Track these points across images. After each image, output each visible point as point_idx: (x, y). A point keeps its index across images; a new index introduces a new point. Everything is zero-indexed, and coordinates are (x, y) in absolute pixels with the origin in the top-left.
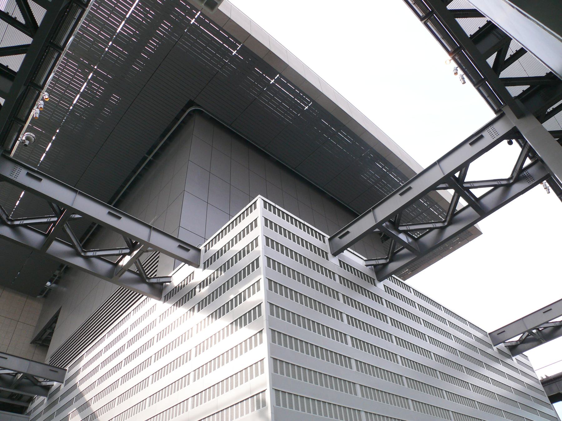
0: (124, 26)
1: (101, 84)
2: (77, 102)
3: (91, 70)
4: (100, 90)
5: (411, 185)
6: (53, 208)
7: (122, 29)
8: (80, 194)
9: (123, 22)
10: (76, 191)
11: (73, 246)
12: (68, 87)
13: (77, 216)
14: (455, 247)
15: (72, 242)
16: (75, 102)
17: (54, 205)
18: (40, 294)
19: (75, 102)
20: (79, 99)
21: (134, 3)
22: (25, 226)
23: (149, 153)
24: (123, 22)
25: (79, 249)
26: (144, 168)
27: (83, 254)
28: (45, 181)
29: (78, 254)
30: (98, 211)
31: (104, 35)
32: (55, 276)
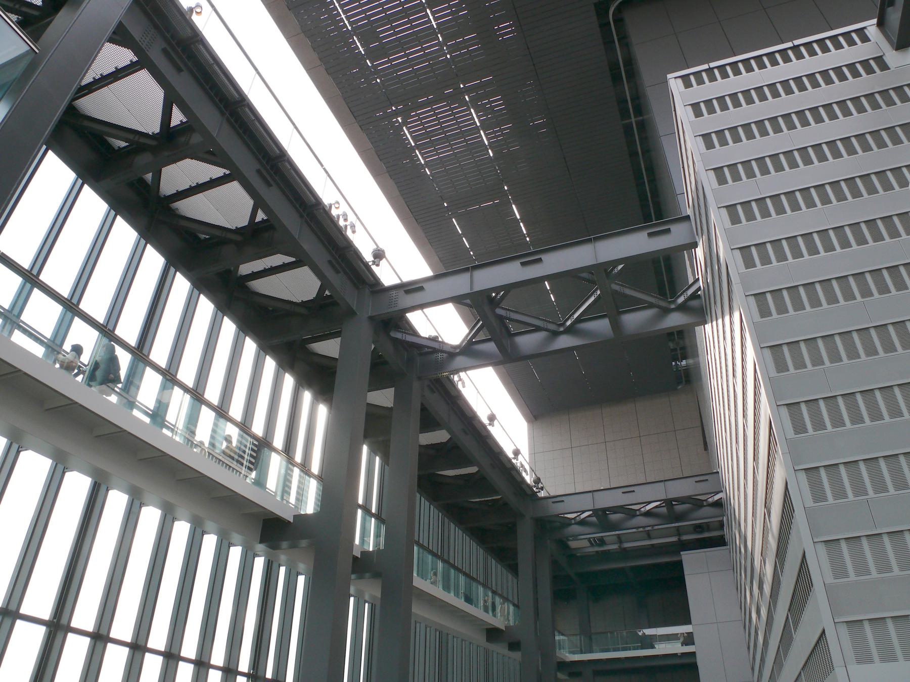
0: (433, 13)
1: (487, 96)
2: (488, 139)
3: (463, 92)
4: (497, 102)
5: (544, 257)
6: (584, 279)
7: (436, 19)
8: (596, 239)
9: (428, 11)
10: (589, 241)
11: (651, 306)
12: (463, 134)
13: (620, 267)
14: (782, 500)
15: (646, 302)
16: (486, 142)
17: (585, 275)
18: (679, 383)
19: (486, 142)
20: (486, 135)
21: (349, 22)
22: (579, 320)
23: (624, 114)
24: (428, 11)
25: (663, 304)
26: (640, 139)
27: (673, 306)
28: (546, 258)
29: (666, 311)
30: (635, 244)
31: (431, 47)
32: (675, 350)
